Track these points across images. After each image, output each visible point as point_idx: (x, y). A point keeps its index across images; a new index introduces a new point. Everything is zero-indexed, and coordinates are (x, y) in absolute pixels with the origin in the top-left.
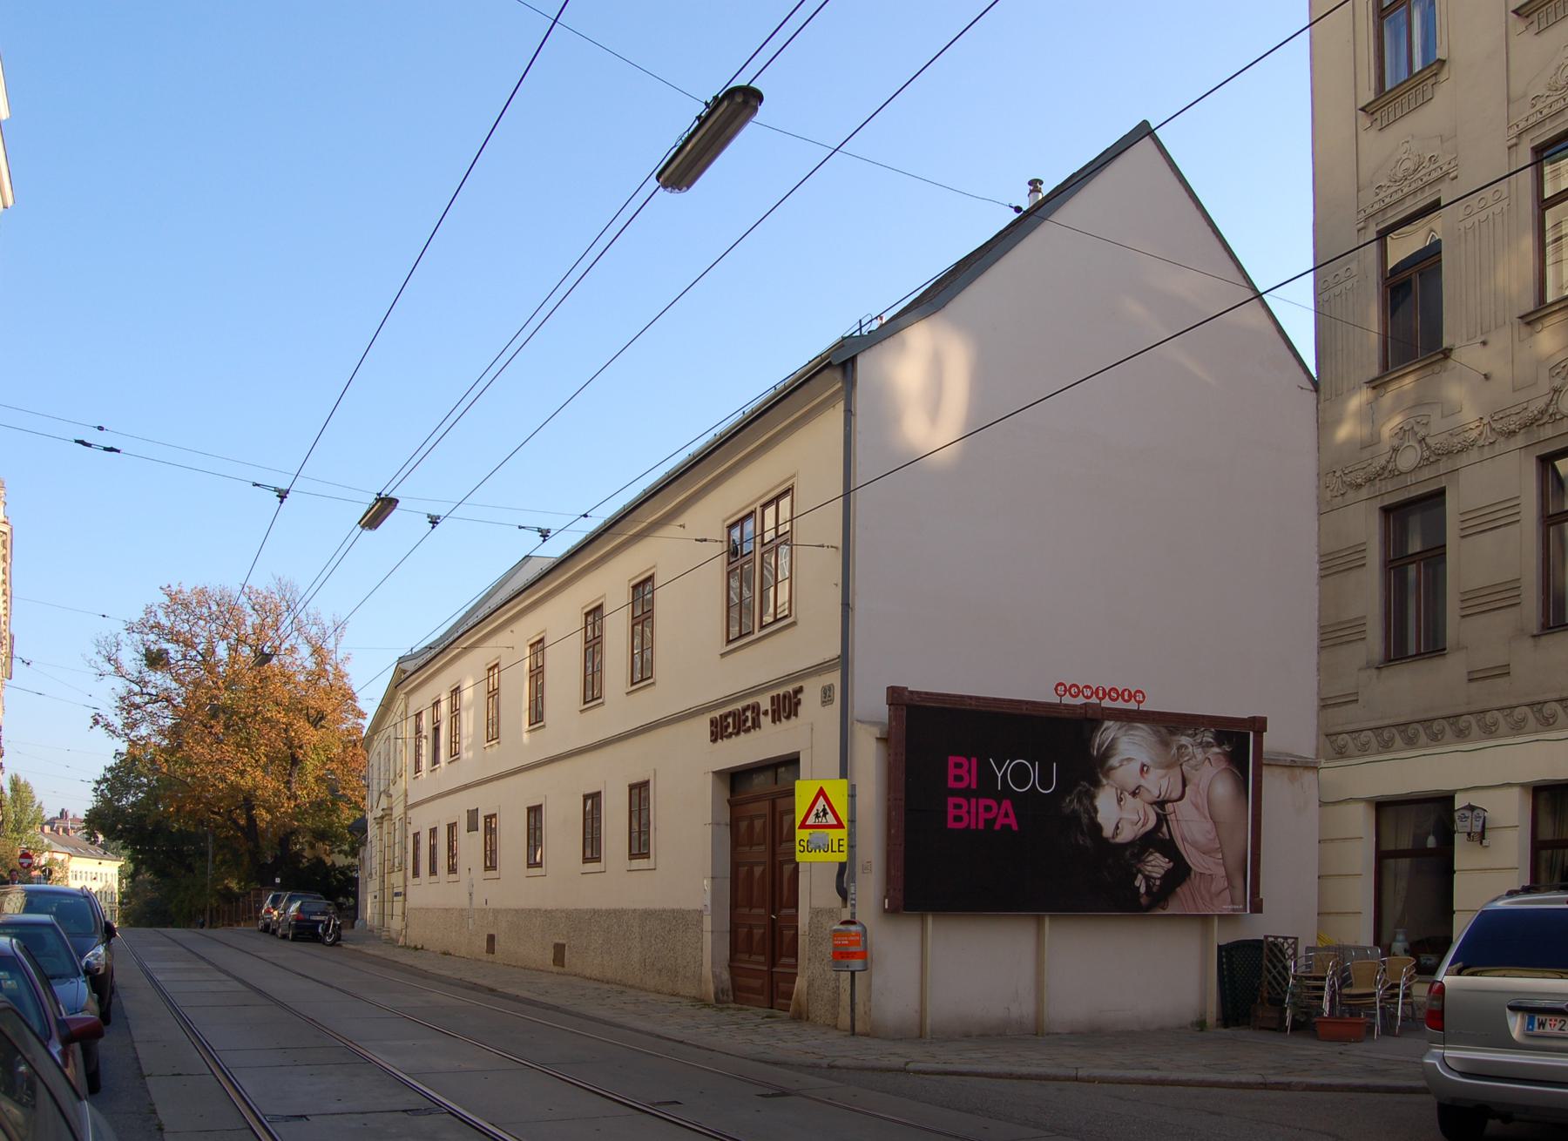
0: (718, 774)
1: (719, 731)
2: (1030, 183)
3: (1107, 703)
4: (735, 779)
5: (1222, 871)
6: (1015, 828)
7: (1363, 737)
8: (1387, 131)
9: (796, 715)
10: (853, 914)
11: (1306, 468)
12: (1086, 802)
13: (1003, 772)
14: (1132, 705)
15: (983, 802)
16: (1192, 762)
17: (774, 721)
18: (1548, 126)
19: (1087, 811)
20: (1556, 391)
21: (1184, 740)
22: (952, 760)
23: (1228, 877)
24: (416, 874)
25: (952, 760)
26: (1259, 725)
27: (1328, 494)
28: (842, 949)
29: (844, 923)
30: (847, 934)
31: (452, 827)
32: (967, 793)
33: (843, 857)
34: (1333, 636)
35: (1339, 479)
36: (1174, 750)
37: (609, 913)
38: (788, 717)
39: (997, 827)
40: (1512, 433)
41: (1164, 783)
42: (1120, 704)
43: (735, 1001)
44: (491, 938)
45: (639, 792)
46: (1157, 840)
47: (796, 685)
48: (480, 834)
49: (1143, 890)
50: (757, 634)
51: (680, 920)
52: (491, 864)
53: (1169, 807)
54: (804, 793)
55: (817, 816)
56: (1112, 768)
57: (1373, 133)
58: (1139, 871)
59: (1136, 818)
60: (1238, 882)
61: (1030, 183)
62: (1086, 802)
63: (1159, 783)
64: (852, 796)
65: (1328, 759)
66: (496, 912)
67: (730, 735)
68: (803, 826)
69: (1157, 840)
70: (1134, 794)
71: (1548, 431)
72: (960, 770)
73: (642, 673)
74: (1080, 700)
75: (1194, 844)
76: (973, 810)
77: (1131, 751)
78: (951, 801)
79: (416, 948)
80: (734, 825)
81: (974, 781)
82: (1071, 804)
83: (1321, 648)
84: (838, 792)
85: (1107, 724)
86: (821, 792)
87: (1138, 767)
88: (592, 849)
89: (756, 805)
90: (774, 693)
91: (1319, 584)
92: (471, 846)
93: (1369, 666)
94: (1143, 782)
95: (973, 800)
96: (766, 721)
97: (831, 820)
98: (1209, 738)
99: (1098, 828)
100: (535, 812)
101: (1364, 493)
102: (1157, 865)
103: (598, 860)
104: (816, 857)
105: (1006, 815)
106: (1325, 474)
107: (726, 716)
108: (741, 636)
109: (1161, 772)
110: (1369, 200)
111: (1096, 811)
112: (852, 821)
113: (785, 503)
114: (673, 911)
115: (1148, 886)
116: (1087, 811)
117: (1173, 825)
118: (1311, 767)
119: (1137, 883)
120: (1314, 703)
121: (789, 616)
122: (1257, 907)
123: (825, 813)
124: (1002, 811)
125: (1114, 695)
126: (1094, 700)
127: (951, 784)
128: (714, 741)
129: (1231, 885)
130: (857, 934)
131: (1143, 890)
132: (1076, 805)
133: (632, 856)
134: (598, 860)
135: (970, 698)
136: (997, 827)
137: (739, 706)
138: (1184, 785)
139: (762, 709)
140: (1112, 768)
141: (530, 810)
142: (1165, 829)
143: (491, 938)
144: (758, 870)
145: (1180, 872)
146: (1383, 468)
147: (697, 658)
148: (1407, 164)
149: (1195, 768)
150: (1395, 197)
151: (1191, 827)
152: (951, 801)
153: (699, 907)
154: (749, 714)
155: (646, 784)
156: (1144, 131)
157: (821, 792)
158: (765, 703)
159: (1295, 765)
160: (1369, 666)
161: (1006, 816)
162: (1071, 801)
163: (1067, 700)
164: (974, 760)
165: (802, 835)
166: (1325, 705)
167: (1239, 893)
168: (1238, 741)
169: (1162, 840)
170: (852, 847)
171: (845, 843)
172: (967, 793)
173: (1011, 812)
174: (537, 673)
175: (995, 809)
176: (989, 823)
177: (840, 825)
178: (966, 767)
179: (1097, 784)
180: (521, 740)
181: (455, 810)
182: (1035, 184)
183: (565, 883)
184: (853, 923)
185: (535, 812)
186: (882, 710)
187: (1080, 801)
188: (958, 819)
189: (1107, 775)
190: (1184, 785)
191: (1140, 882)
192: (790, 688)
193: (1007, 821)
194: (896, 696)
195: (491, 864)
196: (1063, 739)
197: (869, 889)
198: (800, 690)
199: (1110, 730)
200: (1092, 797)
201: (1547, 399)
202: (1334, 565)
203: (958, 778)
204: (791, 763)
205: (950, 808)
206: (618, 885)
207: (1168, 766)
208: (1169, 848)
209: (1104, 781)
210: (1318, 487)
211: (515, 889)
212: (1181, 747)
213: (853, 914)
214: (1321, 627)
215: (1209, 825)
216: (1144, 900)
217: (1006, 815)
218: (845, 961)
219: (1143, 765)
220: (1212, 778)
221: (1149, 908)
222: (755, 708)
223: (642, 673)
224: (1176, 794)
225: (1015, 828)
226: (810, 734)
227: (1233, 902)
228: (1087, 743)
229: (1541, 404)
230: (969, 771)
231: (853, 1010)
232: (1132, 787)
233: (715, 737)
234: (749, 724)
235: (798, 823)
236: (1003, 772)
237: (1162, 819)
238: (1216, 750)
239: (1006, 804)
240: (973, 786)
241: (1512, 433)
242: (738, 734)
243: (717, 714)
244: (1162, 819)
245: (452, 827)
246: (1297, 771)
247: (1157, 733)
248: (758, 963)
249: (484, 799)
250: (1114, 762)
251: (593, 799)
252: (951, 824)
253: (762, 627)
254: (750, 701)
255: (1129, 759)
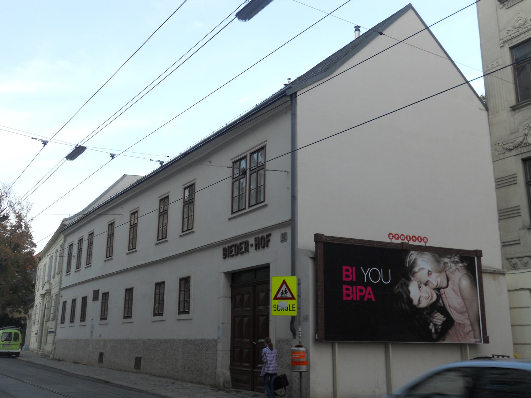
0: (227, 274)
1: (228, 253)
2: (355, 27)
3: (411, 242)
4: (234, 277)
5: (468, 322)
6: (374, 300)
7: (525, 260)
8: (510, 9)
9: (267, 246)
10: (300, 342)
11: (486, 142)
12: (405, 288)
13: (367, 273)
14: (422, 244)
15: (359, 287)
16: (451, 270)
17: (256, 249)
18: (522, 36)
19: (405, 292)
20: (526, 135)
21: (446, 260)
22: (344, 268)
23: (472, 325)
24: (63, 322)
25: (344, 268)
26: (478, 254)
27: (497, 153)
28: (296, 360)
29: (297, 346)
30: (299, 352)
31: (85, 299)
32: (351, 283)
33: (294, 314)
34: (505, 214)
35: (501, 150)
36: (442, 265)
37: (167, 341)
38: (263, 247)
39: (366, 299)
40: (510, 150)
41: (439, 280)
42: (417, 243)
43: (233, 387)
44: (101, 355)
45: (185, 281)
46: (438, 306)
47: (268, 233)
48: (99, 303)
49: (433, 331)
50: (247, 210)
51: (207, 345)
52: (104, 317)
53: (442, 291)
54: (275, 283)
55: (282, 293)
56: (415, 272)
57: (504, 10)
58: (431, 321)
59: (427, 296)
60: (476, 328)
61: (355, 27)
62: (405, 288)
63: (436, 279)
64: (299, 284)
65: (509, 270)
66: (105, 341)
67: (233, 256)
68: (276, 298)
69: (438, 306)
70: (426, 284)
71: (525, 150)
72: (348, 272)
73: (187, 228)
74: (399, 241)
75: (455, 309)
76: (354, 291)
77: (423, 264)
78: (345, 287)
79: (59, 360)
80: (233, 298)
81: (354, 276)
82: (398, 289)
83: (500, 220)
84: (292, 282)
85: (412, 252)
86: (284, 282)
87: (426, 272)
88: (159, 310)
89: (249, 289)
90: (257, 236)
91: (496, 191)
92: (94, 308)
93: (523, 228)
94: (429, 279)
95: (354, 287)
96: (252, 249)
97: (289, 295)
98: (457, 259)
99: (410, 301)
100: (129, 292)
101: (514, 152)
102: (439, 318)
103: (188, 312)
104: (280, 312)
105: (369, 294)
106: (494, 145)
107: (231, 247)
108: (239, 210)
109: (437, 274)
110: (504, 34)
111: (409, 292)
112: (299, 296)
113: (136, 215)
114: (201, 340)
115: (436, 329)
116: (405, 292)
117: (445, 300)
118: (502, 274)
119: (430, 327)
120: (498, 244)
121: (192, 229)
122: (486, 341)
123: (286, 292)
124: (367, 292)
125: (414, 239)
126: (406, 241)
127: (344, 279)
128: (317, 236)
129: (473, 329)
130: (303, 352)
131: (433, 331)
132: (400, 289)
133: (180, 313)
134: (188, 312)
135: (352, 239)
136: (366, 299)
137: (238, 242)
138: (448, 281)
139: (250, 243)
140: (415, 272)
141: (181, 280)
142: (441, 301)
143: (101, 355)
144: (246, 320)
145: (449, 322)
146: (522, 142)
147: (215, 219)
148: (520, 22)
149: (452, 273)
150: (516, 34)
151: (452, 300)
152: (345, 287)
153: (215, 337)
154: (243, 246)
155: (163, 283)
156: (409, 7)
157: (284, 282)
158: (252, 241)
159: (494, 273)
160: (523, 228)
161: (369, 294)
162: (398, 288)
163: (394, 241)
164: (354, 268)
165: (273, 303)
166: (504, 245)
167: (477, 333)
168: (470, 260)
169: (440, 307)
170: (299, 308)
171: (295, 306)
172: (351, 283)
173: (371, 292)
174: (134, 227)
175: (364, 292)
176: (362, 297)
177: (293, 298)
178: (350, 271)
179: (409, 280)
180: (122, 258)
181: (88, 291)
182: (357, 28)
183: (144, 326)
184: (301, 346)
185: (129, 292)
186: (311, 245)
187: (402, 287)
188: (348, 295)
189: (413, 276)
190: (448, 281)
191: (431, 327)
192: (265, 235)
193: (369, 297)
194: (318, 238)
195: (104, 317)
196: (393, 258)
197: (308, 329)
198: (270, 235)
199: (413, 255)
200: (407, 286)
201: (522, 138)
202: (503, 183)
203: (347, 276)
204: (265, 268)
205: (344, 290)
206: (172, 327)
207: (440, 272)
208: (444, 311)
209: (412, 278)
210: (492, 150)
211: (116, 329)
212: (445, 263)
213: (300, 342)
214: (499, 210)
215: (460, 300)
216: (434, 336)
217: (369, 294)
218: (298, 366)
219: (429, 271)
220: (460, 278)
221: (437, 340)
222: (247, 243)
223: (187, 228)
224: (444, 285)
225: (374, 300)
226: (275, 255)
227: (475, 338)
228: (404, 260)
229: (521, 139)
230: (352, 273)
231: (301, 392)
232: (425, 281)
233: (225, 256)
234: (243, 250)
235: (273, 297)
236: (367, 273)
237: (439, 297)
238: (461, 265)
239: (369, 288)
240: (354, 280)
241: (510, 150)
242: (237, 255)
243: (226, 246)
244: (439, 297)
245: (85, 299)
246: (497, 276)
247: (434, 256)
248: (246, 367)
249: (102, 287)
250: (416, 269)
251: (160, 286)
252: (345, 298)
253: (250, 206)
254: (244, 240)
255: (423, 268)
